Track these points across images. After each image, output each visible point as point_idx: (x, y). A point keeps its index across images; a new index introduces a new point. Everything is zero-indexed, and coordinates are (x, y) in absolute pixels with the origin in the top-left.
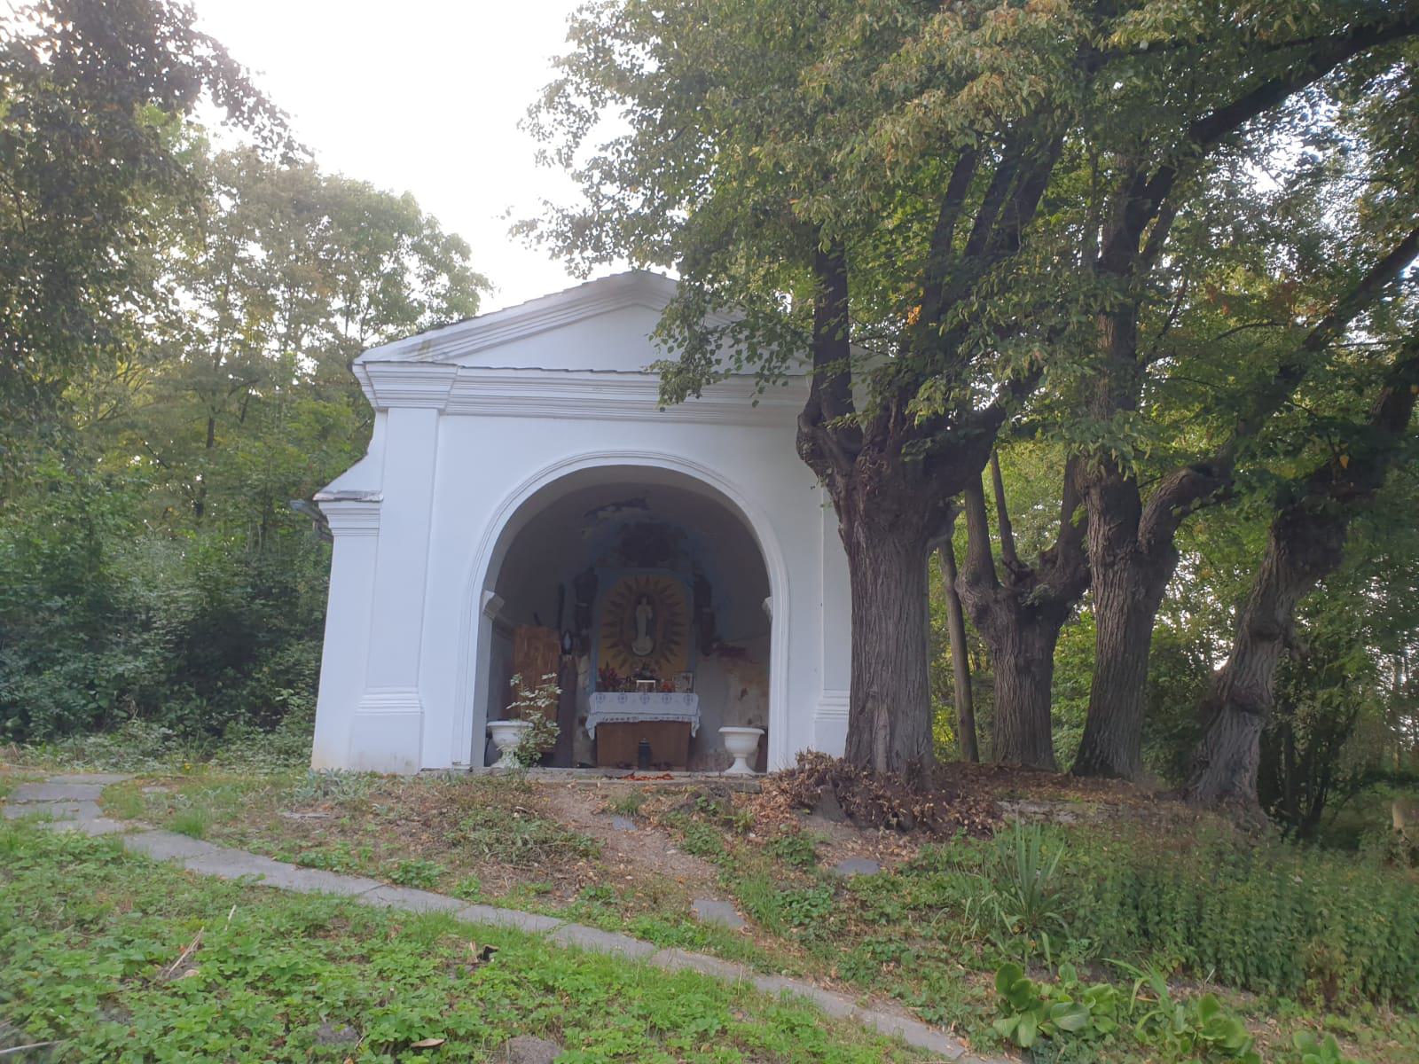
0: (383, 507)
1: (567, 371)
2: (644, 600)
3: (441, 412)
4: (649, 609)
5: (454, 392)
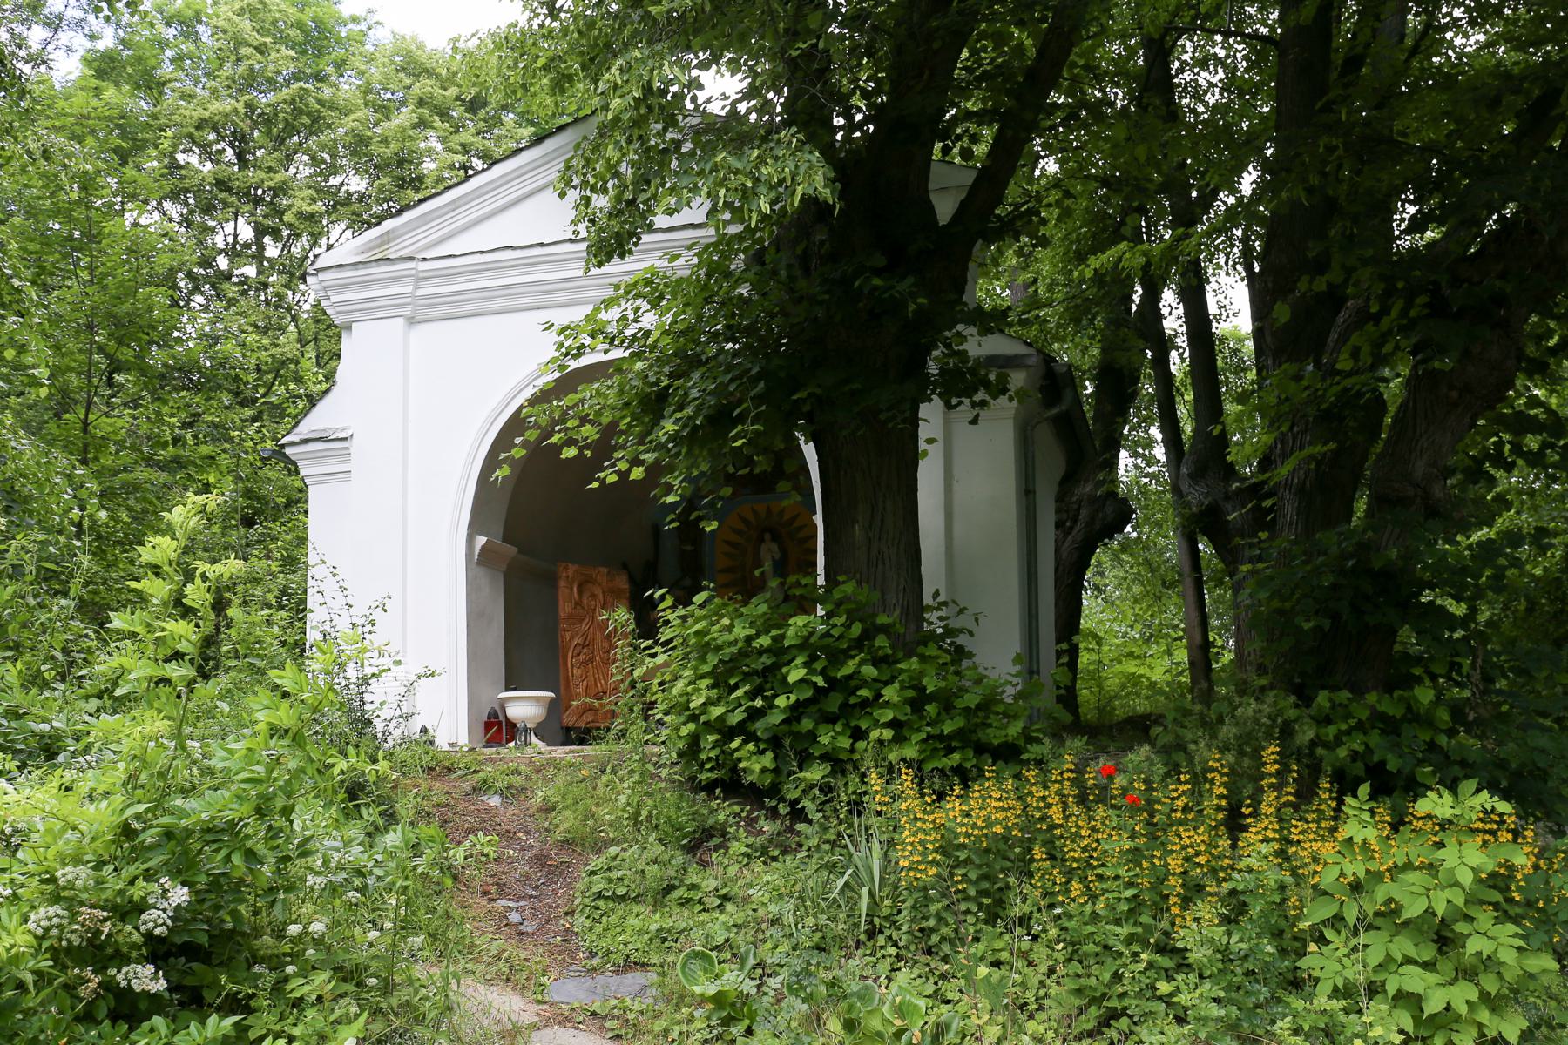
0: (354, 446)
1: (542, 245)
2: (767, 536)
3: (412, 321)
4: (775, 547)
5: (420, 292)
